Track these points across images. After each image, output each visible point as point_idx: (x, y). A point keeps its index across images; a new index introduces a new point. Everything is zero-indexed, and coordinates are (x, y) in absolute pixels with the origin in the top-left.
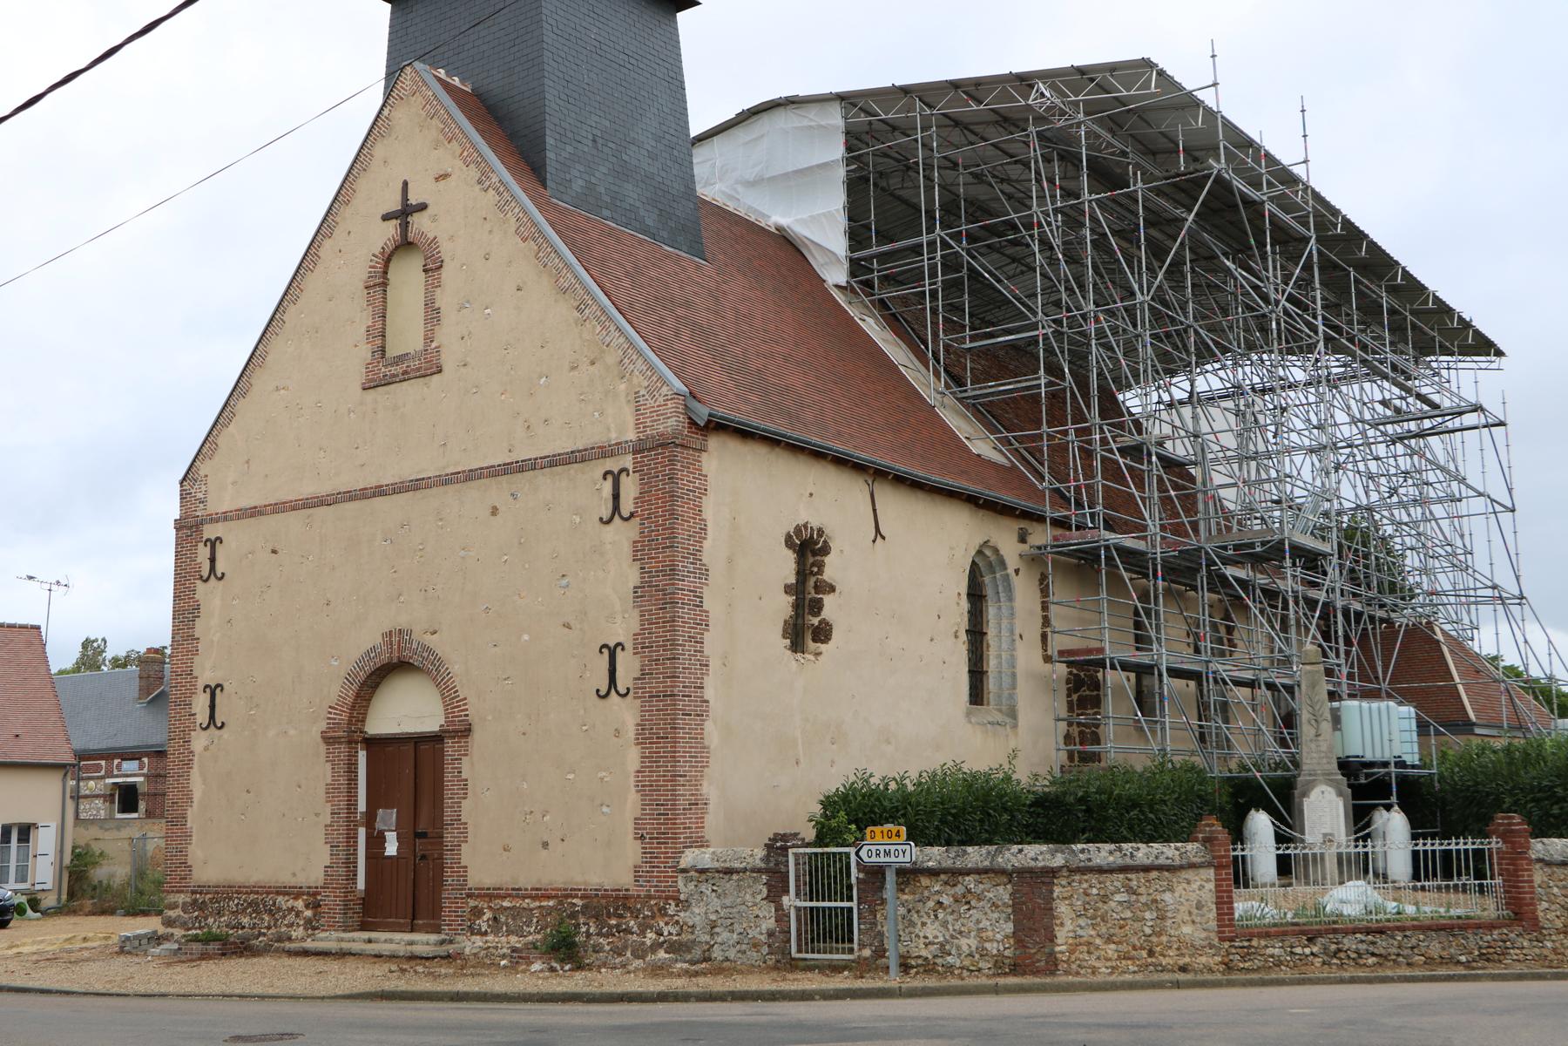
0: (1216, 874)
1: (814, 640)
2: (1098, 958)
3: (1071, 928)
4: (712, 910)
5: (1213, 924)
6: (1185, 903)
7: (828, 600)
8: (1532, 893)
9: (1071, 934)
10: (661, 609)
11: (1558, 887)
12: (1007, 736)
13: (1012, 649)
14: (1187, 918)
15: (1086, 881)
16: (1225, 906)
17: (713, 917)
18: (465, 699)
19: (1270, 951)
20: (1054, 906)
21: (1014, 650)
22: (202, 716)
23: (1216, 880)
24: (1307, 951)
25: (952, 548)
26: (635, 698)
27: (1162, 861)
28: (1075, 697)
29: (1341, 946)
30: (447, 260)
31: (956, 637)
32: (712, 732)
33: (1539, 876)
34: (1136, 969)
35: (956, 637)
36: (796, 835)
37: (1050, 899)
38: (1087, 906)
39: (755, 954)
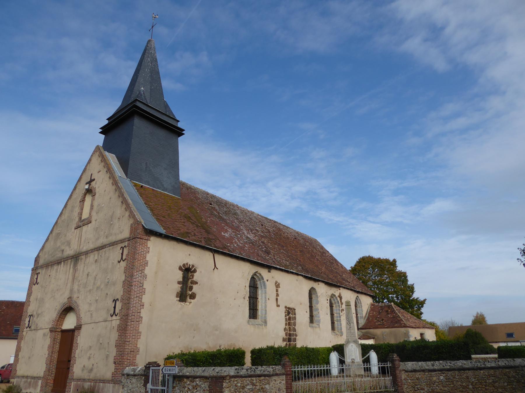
1: (190, 299)
6: (274, 389)
7: (195, 287)
10: (128, 288)
11: (410, 380)
12: (263, 328)
13: (266, 302)
15: (236, 381)
16: (289, 390)
18: (81, 318)
20: (223, 390)
21: (266, 303)
22: (27, 325)
23: (286, 380)
26: (119, 316)
27: (266, 373)
28: (288, 317)
30: (97, 193)
31: (244, 298)
32: (142, 328)
33: (404, 376)
35: (244, 298)
37: (222, 388)
38: (236, 391)
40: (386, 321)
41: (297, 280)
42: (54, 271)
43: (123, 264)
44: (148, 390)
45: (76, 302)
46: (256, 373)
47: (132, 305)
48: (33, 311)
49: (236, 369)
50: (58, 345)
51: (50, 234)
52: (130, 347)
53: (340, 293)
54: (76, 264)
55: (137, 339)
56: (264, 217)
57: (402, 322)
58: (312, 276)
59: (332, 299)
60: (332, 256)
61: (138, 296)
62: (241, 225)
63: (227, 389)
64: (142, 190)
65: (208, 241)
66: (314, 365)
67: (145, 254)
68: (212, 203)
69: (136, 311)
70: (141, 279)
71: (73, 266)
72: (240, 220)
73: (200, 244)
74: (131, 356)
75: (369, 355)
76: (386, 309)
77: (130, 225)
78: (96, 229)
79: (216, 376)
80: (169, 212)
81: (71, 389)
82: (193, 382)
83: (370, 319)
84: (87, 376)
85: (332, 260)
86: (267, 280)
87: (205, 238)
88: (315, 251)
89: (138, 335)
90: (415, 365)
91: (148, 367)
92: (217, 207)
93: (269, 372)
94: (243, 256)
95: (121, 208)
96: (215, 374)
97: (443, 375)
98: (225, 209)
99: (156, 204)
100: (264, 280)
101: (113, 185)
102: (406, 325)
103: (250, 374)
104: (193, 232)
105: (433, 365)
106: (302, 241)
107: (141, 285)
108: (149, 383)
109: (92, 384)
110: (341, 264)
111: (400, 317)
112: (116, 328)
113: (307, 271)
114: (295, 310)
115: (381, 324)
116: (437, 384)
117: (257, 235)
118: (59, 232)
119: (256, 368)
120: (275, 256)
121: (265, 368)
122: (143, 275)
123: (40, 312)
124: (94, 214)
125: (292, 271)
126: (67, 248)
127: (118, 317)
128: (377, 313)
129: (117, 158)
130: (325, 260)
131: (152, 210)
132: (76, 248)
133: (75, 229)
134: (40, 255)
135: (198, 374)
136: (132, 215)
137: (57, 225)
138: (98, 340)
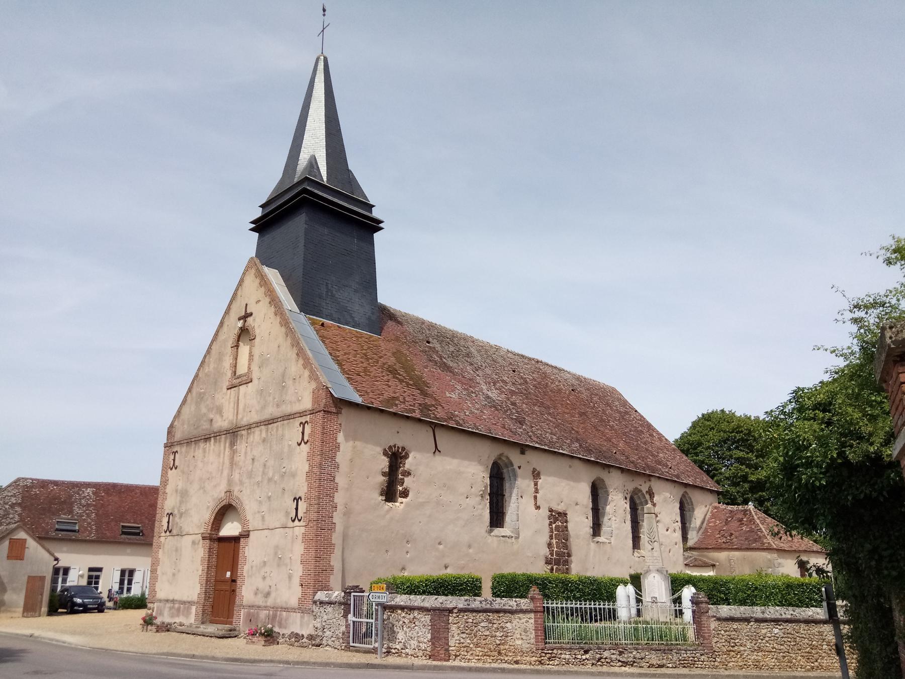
0: (535, 616)
2: (472, 654)
3: (458, 638)
4: (323, 621)
5: (533, 641)
8: (709, 633)
9: (457, 642)
14: (518, 636)
15: (467, 615)
16: (539, 632)
17: (324, 624)
18: (248, 521)
19: (563, 656)
22: (165, 528)
23: (535, 618)
24: (584, 657)
25: (480, 457)
26: (304, 521)
27: (507, 607)
28: (554, 526)
34: (491, 661)
36: (357, 586)
39: (338, 643)
40: (736, 537)
41: (570, 467)
42: (198, 451)
43: (305, 448)
44: (349, 622)
45: (238, 498)
48: (173, 508)
49: (466, 600)
51: (187, 393)
53: (650, 487)
54: (234, 443)
56: (518, 355)
57: (765, 541)
58: (597, 459)
59: (635, 497)
60: (642, 419)
61: (328, 495)
62: (478, 375)
65: (425, 408)
68: (431, 340)
71: (229, 445)
72: (475, 365)
73: (413, 415)
75: (673, 595)
76: (740, 516)
77: (311, 391)
78: (261, 392)
79: (439, 608)
80: (365, 365)
81: (241, 620)
82: (410, 614)
83: (708, 532)
84: (262, 602)
85: (642, 425)
86: (519, 467)
87: (420, 405)
88: (609, 411)
89: (331, 549)
90: (733, 610)
91: (348, 593)
92: (438, 346)
93: (512, 606)
94: (480, 431)
95: (297, 364)
96: (438, 605)
97: (779, 627)
98: (452, 349)
99: (345, 354)
100: (514, 467)
101: (281, 326)
102: (771, 545)
104: (401, 395)
105: (763, 613)
106: (585, 395)
108: (350, 613)
109: (271, 613)
110: (659, 434)
111: (762, 532)
112: (300, 538)
113: (589, 451)
114: (565, 514)
115: (728, 542)
116: (767, 639)
117: (504, 390)
118: (203, 390)
120: (533, 427)
123: (183, 509)
124: (255, 368)
125: (561, 451)
126: (218, 417)
127: (302, 523)
128: (721, 523)
129: (282, 277)
130: (627, 427)
131: (340, 364)
132: (231, 417)
133: (228, 389)
134: (175, 424)
135: (416, 604)
136: (313, 377)
137: (198, 380)
138: (276, 553)
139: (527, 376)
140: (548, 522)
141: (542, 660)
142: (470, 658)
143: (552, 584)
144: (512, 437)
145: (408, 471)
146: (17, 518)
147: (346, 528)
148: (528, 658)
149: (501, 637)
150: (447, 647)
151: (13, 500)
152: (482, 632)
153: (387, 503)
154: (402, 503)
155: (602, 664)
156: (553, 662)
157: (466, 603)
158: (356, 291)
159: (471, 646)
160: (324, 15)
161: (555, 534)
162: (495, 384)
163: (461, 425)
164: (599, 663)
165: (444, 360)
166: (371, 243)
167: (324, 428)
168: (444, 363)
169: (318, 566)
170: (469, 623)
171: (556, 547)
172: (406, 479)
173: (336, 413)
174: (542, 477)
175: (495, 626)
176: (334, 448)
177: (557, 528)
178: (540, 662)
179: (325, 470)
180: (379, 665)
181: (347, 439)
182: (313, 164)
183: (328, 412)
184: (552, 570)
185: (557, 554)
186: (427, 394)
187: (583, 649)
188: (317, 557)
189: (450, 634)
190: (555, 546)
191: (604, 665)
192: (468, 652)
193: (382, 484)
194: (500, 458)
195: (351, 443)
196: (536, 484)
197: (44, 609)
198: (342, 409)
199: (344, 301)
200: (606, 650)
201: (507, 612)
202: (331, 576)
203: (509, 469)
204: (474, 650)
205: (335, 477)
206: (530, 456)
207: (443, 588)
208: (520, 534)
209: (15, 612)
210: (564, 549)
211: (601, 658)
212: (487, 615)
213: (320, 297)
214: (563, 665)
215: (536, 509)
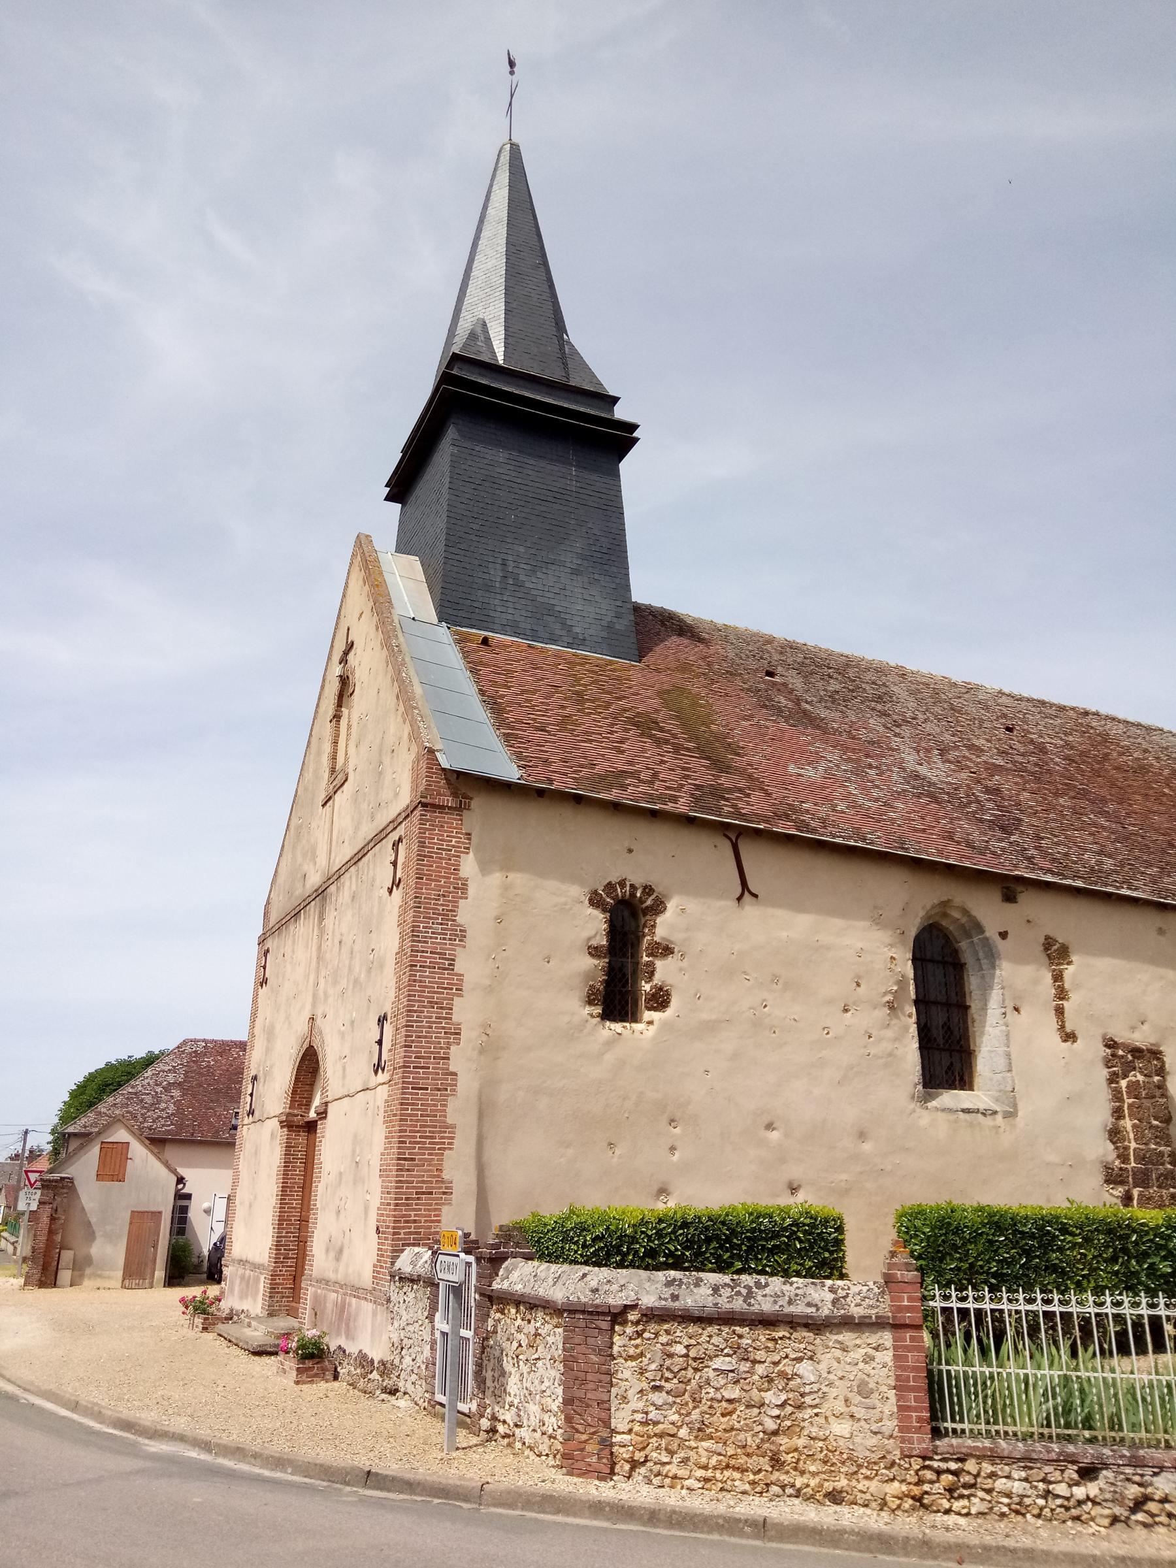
2: (685, 1461)
3: (640, 1405)
5: (890, 1425)
6: (838, 1383)
9: (639, 1417)
14: (840, 1407)
15: (667, 1332)
19: (1000, 1484)
23: (895, 1348)
24: (1079, 1492)
27: (799, 1309)
28: (1123, 1083)
29: (1150, 1490)
34: (747, 1487)
41: (1161, 931)
46: (756, 1308)
47: (415, 1031)
49: (669, 1284)
50: (299, 1167)
52: (415, 1176)
55: (439, 1149)
63: (630, 1363)
64: (484, 654)
66: (1028, 1288)
67: (454, 856)
69: (432, 1053)
70: (446, 944)
73: (669, 807)
74: (420, 1210)
93: (816, 1305)
94: (868, 844)
96: (584, 1297)
100: (987, 934)
103: (728, 1306)
107: (444, 964)
119: (758, 1285)
121: (798, 1288)
122: (452, 930)
125: (1125, 892)
139: (1048, 740)
140: (1105, 1073)
141: (926, 1493)
142: (681, 1473)
143: (1072, 1234)
144: (969, 858)
145: (665, 943)
146: (172, 1108)
147: (488, 1086)
148: (874, 1486)
149: (782, 1406)
150: (605, 1433)
151: (171, 1078)
152: (717, 1389)
153: (608, 1023)
154: (650, 1023)
155: (1149, 1520)
156: (965, 1502)
157: (667, 1292)
158: (575, 572)
159: (683, 1432)
160: (512, 73)
161: (1130, 1106)
162: (943, 752)
163: (814, 831)
164: (1140, 1517)
165: (808, 707)
166: (616, 475)
167: (422, 844)
168: (805, 712)
169: (407, 1182)
170: (676, 1359)
171: (1136, 1140)
172: (659, 964)
173: (455, 809)
174: (1074, 958)
175: (760, 1369)
176: (452, 889)
177: (1133, 1088)
178: (918, 1499)
179: (426, 942)
180: (394, 1479)
181: (485, 867)
182: (480, 332)
183: (434, 806)
184: (1127, 1199)
185: (1140, 1158)
186: (729, 767)
187: (1073, 1462)
188: (405, 1159)
189: (614, 1390)
190: (1132, 1136)
191: (1157, 1523)
192: (672, 1453)
193: (588, 976)
194: (945, 915)
195: (496, 878)
196: (1058, 977)
197: (160, 1274)
198: (471, 799)
199: (548, 595)
200: (1162, 1468)
201: (799, 1324)
202: (445, 1209)
203: (975, 940)
204: (690, 1448)
205: (454, 960)
206: (1030, 904)
207: (714, 1244)
208: (1020, 1106)
209: (109, 1278)
210: (1157, 1144)
211: (1147, 1498)
212: (734, 1332)
213: (488, 588)
214: (1003, 1515)
215: (1065, 1041)
